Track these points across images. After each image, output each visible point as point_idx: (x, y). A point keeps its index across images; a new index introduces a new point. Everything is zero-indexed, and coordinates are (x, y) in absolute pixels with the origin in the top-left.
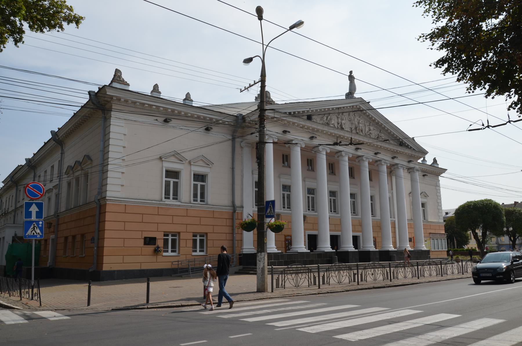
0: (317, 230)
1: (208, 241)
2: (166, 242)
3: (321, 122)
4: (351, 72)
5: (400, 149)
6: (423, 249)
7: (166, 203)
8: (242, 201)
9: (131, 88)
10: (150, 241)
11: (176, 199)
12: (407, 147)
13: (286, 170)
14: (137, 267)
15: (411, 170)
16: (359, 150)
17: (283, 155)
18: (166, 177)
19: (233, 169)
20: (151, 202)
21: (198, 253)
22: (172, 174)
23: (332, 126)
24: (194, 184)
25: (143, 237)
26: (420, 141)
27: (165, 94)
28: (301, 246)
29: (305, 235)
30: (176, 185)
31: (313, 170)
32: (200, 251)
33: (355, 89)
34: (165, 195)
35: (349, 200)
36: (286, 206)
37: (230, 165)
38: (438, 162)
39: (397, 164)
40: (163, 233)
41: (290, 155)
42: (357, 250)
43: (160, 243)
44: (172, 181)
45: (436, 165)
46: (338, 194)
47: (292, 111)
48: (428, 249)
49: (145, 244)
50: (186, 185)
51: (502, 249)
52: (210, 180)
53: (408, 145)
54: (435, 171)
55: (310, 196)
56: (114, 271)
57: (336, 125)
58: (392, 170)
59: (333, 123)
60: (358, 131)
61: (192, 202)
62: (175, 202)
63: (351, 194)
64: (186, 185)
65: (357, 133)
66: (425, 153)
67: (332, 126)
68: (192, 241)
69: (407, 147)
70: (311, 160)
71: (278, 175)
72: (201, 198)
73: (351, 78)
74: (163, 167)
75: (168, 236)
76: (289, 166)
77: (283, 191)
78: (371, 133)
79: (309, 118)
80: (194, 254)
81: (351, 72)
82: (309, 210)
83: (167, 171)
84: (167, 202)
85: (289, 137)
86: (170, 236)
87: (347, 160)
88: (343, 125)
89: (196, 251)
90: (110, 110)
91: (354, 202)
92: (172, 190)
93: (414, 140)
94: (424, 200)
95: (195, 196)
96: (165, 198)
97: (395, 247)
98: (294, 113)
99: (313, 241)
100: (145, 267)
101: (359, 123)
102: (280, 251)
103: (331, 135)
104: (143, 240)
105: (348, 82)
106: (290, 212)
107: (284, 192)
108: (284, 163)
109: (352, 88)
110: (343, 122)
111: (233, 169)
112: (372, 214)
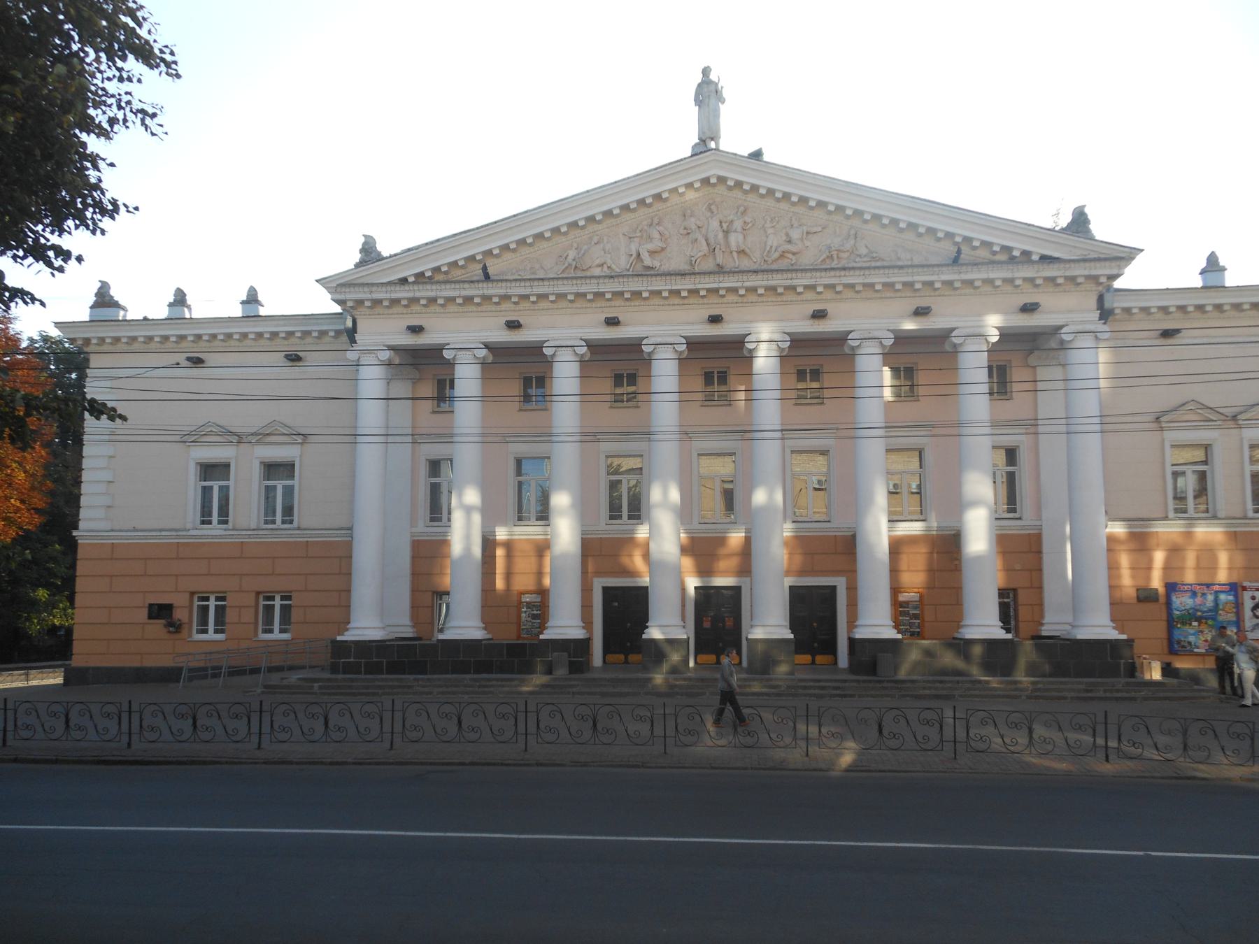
10: (161, 611)
13: (624, 417)
14: (134, 663)
22: (211, 470)
27: (201, 308)
32: (216, 632)
42: (1009, 636)
43: (179, 614)
44: (279, 485)
47: (426, 267)
49: (150, 617)
50: (246, 490)
51: (730, 592)
56: (87, 669)
61: (1251, 514)
64: (246, 490)
67: (597, 272)
72: (219, 515)
74: (1163, 441)
84: (207, 531)
85: (935, 323)
86: (278, 598)
92: (214, 507)
95: (270, 510)
98: (437, 270)
100: (149, 663)
104: (145, 612)
105: (692, 113)
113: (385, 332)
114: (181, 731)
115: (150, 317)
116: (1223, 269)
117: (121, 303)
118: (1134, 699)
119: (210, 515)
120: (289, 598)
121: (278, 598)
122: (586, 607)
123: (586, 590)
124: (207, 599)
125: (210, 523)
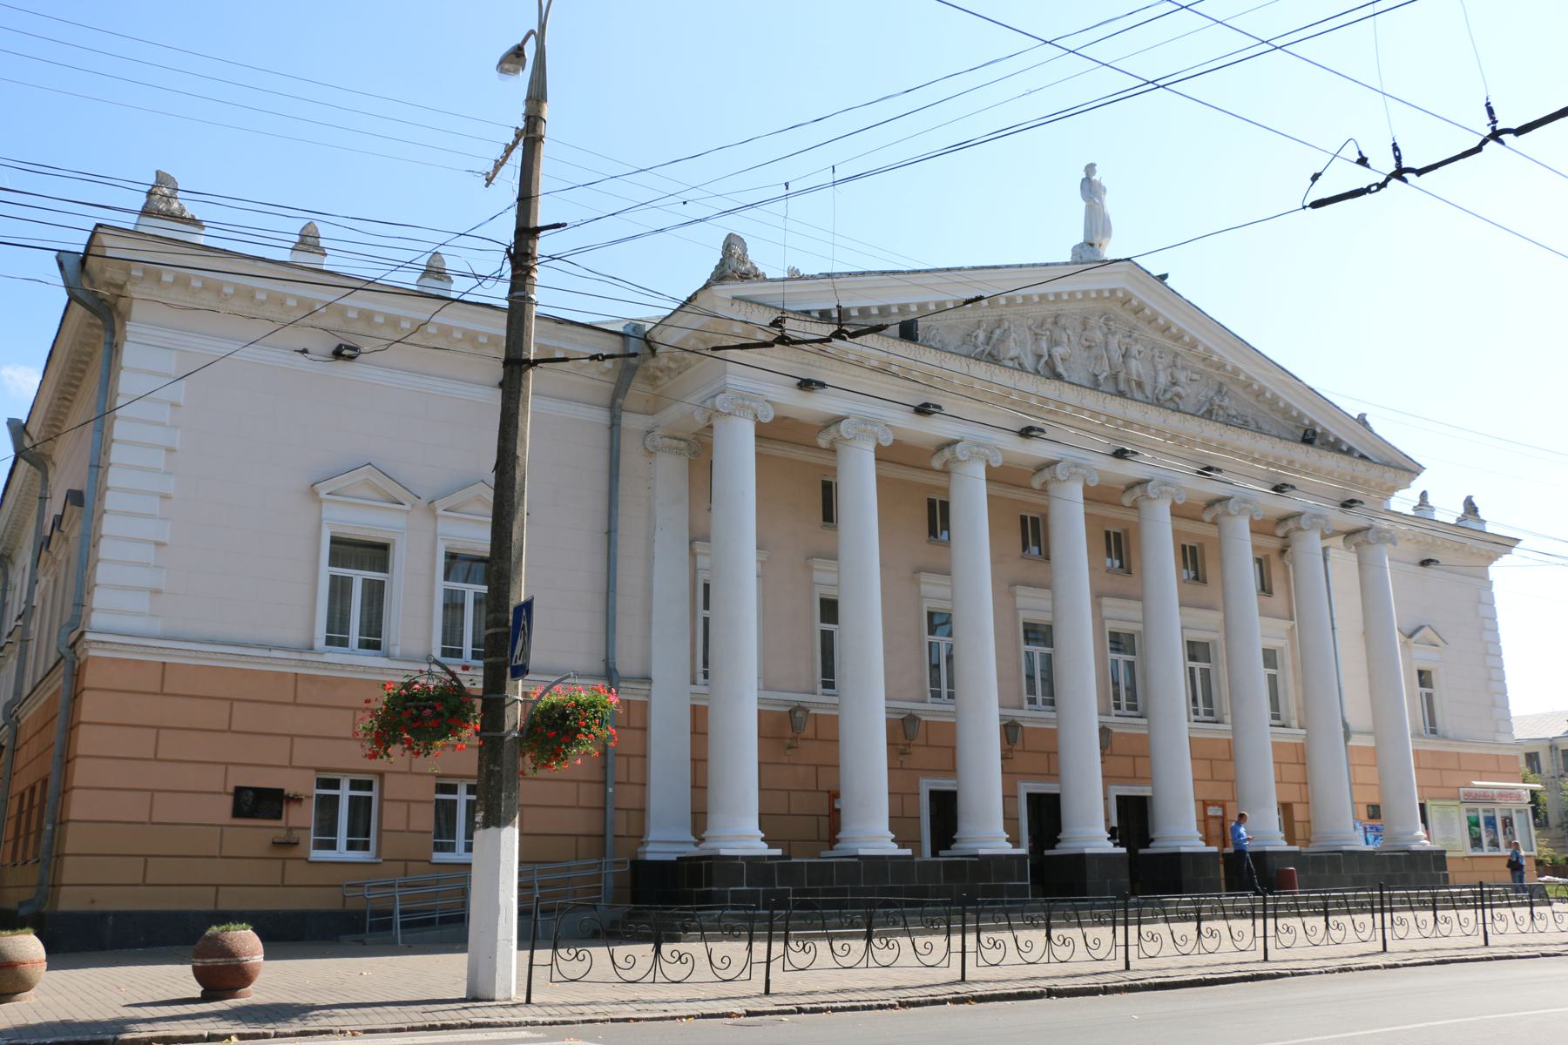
0: (1148, 779)
1: (385, 804)
2: (327, 806)
3: (964, 350)
4: (1090, 168)
5: (1302, 453)
6: (1415, 847)
7: (328, 658)
8: (647, 658)
9: (1489, 528)
10: (258, 803)
11: (376, 646)
12: (1335, 446)
15: (1358, 538)
16: (1356, 510)
17: (1023, 520)
18: (331, 564)
19: (611, 533)
20: (266, 653)
21: (341, 853)
23: (1010, 364)
24: (333, 578)
25: (231, 789)
26: (1391, 429)
28: (989, 831)
29: (1106, 799)
30: (375, 594)
31: (1126, 568)
33: (1106, 230)
34: (444, 643)
35: (1262, 673)
36: (1039, 697)
37: (601, 523)
38: (1482, 514)
39: (1296, 516)
40: (433, 782)
41: (1045, 516)
44: (358, 577)
45: (1472, 524)
46: (1060, 635)
48: (1437, 847)
49: (238, 812)
52: (398, 558)
53: (1338, 441)
54: (1470, 545)
55: (1197, 665)
56: (104, 915)
57: (1029, 362)
58: (1279, 539)
59: (1012, 354)
60: (1122, 387)
62: (370, 659)
63: (1191, 645)
65: (1121, 394)
66: (1408, 469)
67: (1010, 364)
68: (432, 808)
69: (1335, 446)
70: (1035, 521)
71: (1006, 588)
73: (1090, 188)
75: (337, 787)
76: (1046, 556)
77: (1027, 640)
78: (1178, 395)
79: (908, 332)
80: (439, 857)
81: (1090, 168)
82: (1032, 701)
83: (335, 541)
84: (336, 656)
86: (462, 789)
87: (983, 475)
88: (1058, 363)
89: (332, 845)
90: (125, 317)
91: (1429, 697)
92: (358, 612)
93: (1365, 424)
94: (1424, 657)
96: (330, 641)
97: (1290, 839)
99: (1133, 818)
101: (1125, 355)
102: (778, 852)
103: (1004, 398)
104: (228, 802)
105: (1081, 206)
106: (1053, 715)
107: (1031, 648)
108: (1025, 546)
109: (1097, 224)
110: (1058, 352)
111: (611, 533)
112: (1276, 717)
113: (764, 384)
114: (1185, 938)
115: (1373, 424)
116: (1470, 545)
117: (761, 270)
118: (266, 1036)
119: (345, 628)
120: (368, 786)
121: (462, 789)
122: (1010, 822)
123: (1009, 797)
124: (335, 784)
125: (344, 643)
